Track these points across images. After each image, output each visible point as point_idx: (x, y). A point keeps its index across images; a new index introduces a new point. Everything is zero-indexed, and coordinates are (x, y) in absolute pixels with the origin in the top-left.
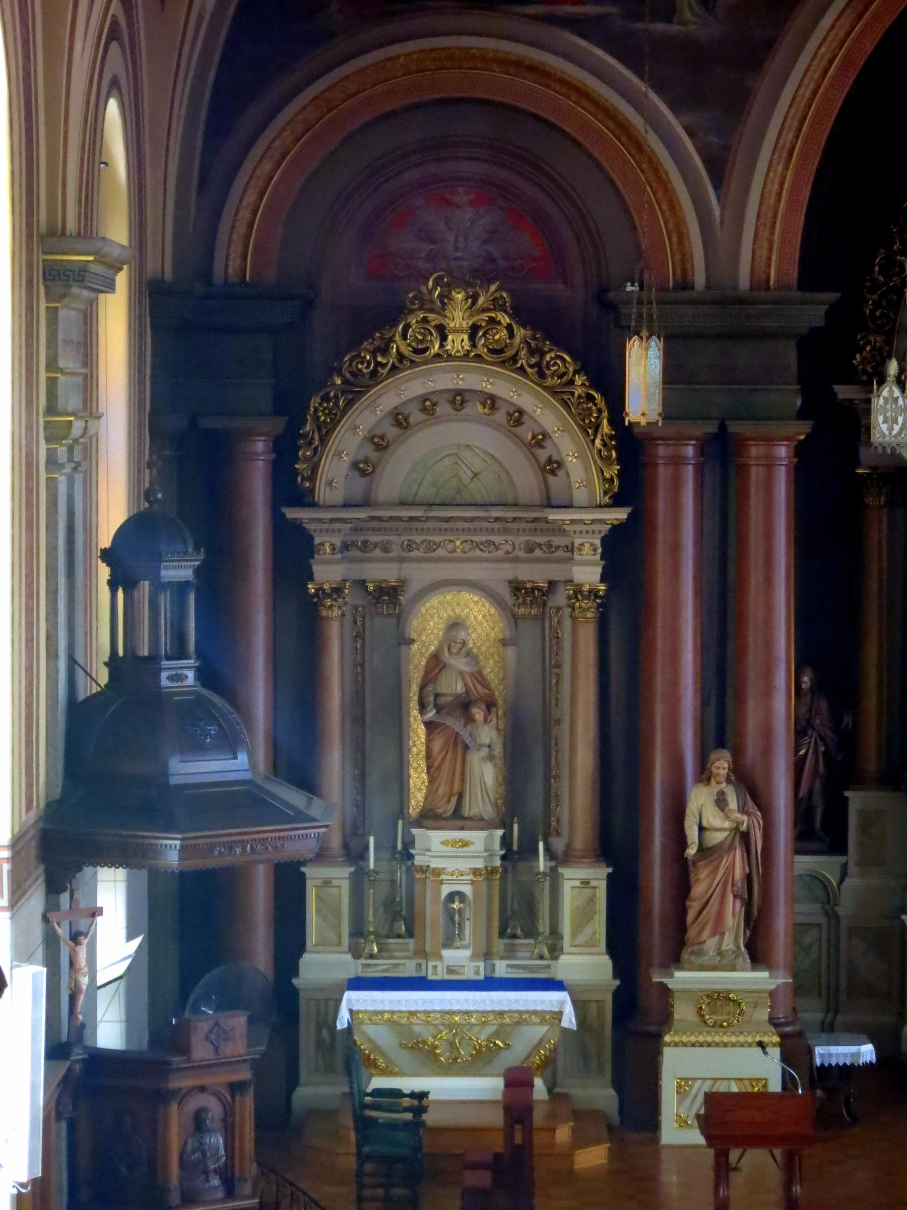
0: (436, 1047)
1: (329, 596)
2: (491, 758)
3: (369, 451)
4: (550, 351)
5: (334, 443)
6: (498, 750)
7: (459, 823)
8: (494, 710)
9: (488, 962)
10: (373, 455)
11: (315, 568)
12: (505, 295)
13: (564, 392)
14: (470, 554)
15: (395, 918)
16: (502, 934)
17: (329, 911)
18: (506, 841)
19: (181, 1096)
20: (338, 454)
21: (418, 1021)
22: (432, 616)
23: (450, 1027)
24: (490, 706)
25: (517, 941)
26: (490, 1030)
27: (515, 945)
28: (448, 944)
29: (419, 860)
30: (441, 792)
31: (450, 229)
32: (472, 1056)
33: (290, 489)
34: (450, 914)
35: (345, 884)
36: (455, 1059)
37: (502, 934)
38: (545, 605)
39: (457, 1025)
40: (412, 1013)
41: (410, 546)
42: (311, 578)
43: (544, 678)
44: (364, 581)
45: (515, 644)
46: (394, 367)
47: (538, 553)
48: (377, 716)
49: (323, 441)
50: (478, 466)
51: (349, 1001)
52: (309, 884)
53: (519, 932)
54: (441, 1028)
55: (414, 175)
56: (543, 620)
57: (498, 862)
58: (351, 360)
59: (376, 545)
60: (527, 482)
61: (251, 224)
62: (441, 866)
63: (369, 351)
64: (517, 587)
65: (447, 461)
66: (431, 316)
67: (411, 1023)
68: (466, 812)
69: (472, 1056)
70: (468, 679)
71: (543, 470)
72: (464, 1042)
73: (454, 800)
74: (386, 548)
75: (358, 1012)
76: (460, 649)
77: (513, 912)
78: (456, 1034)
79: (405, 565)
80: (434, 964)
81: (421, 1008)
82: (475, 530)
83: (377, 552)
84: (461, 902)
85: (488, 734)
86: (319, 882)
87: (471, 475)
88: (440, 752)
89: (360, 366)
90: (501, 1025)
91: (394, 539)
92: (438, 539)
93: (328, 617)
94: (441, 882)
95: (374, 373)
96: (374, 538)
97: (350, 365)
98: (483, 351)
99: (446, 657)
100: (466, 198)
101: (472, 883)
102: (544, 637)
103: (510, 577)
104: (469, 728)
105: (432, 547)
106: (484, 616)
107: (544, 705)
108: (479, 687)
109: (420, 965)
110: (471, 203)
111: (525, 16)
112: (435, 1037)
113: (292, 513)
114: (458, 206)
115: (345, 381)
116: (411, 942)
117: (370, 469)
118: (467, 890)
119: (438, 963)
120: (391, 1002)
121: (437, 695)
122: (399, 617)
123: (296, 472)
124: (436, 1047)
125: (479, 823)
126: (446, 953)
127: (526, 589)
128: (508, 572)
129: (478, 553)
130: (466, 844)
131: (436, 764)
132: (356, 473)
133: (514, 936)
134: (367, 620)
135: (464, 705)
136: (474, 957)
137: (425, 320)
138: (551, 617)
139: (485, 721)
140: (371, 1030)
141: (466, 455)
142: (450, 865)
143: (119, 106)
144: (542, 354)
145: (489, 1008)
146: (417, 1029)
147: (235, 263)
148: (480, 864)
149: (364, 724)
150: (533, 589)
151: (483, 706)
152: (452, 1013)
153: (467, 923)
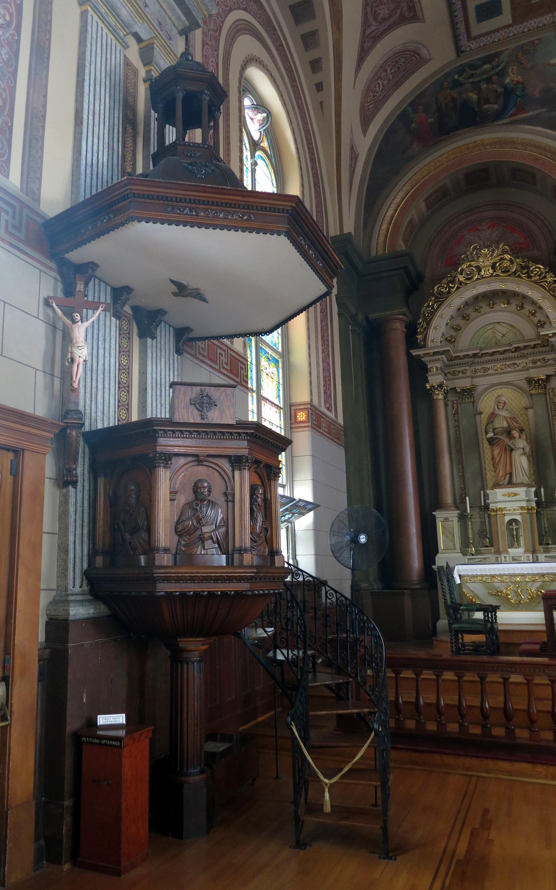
0: (508, 595)
1: (437, 389)
2: (525, 454)
3: (452, 332)
4: (533, 265)
5: (433, 324)
6: (527, 450)
7: (512, 486)
8: (524, 432)
9: (534, 555)
10: (454, 334)
11: (429, 378)
12: (507, 247)
13: (541, 282)
14: (505, 370)
15: (484, 539)
16: (541, 544)
17: (449, 533)
18: (537, 494)
19: (167, 458)
20: (435, 328)
21: (496, 581)
22: (490, 401)
23: (515, 583)
24: (521, 431)
25: (549, 546)
26: (537, 584)
27: (548, 548)
28: (512, 546)
29: (492, 506)
30: (500, 474)
31: (481, 240)
32: (529, 599)
33: (412, 338)
34: (510, 530)
35: (456, 519)
36: (520, 602)
37: (541, 544)
38: (545, 388)
39: (519, 582)
40: (493, 576)
41: (476, 371)
42: (428, 382)
43: (549, 422)
44: (455, 388)
45: (532, 408)
46: (458, 288)
47: (539, 364)
48: (466, 447)
49: (428, 324)
50: (504, 331)
51: (458, 570)
52: (437, 520)
53: (550, 542)
54: (510, 584)
55: (463, 222)
56: (545, 394)
57: (534, 504)
58: (438, 288)
59: (459, 372)
60: (528, 331)
61: (386, 236)
62: (503, 507)
63: (445, 283)
64: (530, 381)
65: (490, 332)
66: (472, 263)
67: (493, 582)
68: (514, 480)
69: (529, 599)
70: (509, 420)
71: (537, 327)
72: (524, 592)
73: (508, 476)
74: (464, 372)
75: (465, 576)
76: (504, 407)
77: (546, 532)
78: (519, 587)
79: (474, 380)
80: (505, 555)
81: (497, 573)
82: (506, 358)
83: (460, 375)
84: (517, 524)
85: (521, 443)
86: (442, 519)
87: (502, 336)
88: (498, 454)
89: (442, 290)
90: (543, 582)
91: (468, 368)
92: (488, 366)
93: (437, 399)
94: (504, 515)
95: (449, 292)
96: (458, 369)
97: (438, 290)
98: (499, 272)
99: (497, 412)
100: (486, 226)
101: (521, 514)
102: (547, 401)
103: (526, 376)
104: (512, 441)
105: (485, 370)
106: (515, 398)
107: (551, 434)
108: (515, 424)
109: (497, 558)
110: (489, 228)
111: (499, 125)
112: (506, 589)
113: (415, 353)
114: (483, 230)
115: (436, 298)
116: (492, 549)
117: (453, 340)
118: (519, 518)
119: (507, 556)
120: (480, 570)
121: (494, 429)
122: (474, 402)
123: (417, 339)
124: (508, 595)
125: (522, 485)
126: (510, 550)
127: (534, 380)
128: (525, 375)
129: (509, 369)
130: (516, 495)
131: (497, 461)
132: (447, 343)
133: (548, 544)
134: (459, 406)
135: (508, 433)
136: (526, 551)
137: (470, 266)
138: (549, 393)
139: (520, 437)
140: (471, 586)
141: (498, 327)
142: (509, 506)
143: (275, 89)
144: (528, 268)
145: (535, 572)
146: (497, 585)
147: (380, 252)
148: (524, 504)
149: (461, 452)
150: (539, 380)
151: (518, 430)
152: (516, 575)
153: (521, 538)
